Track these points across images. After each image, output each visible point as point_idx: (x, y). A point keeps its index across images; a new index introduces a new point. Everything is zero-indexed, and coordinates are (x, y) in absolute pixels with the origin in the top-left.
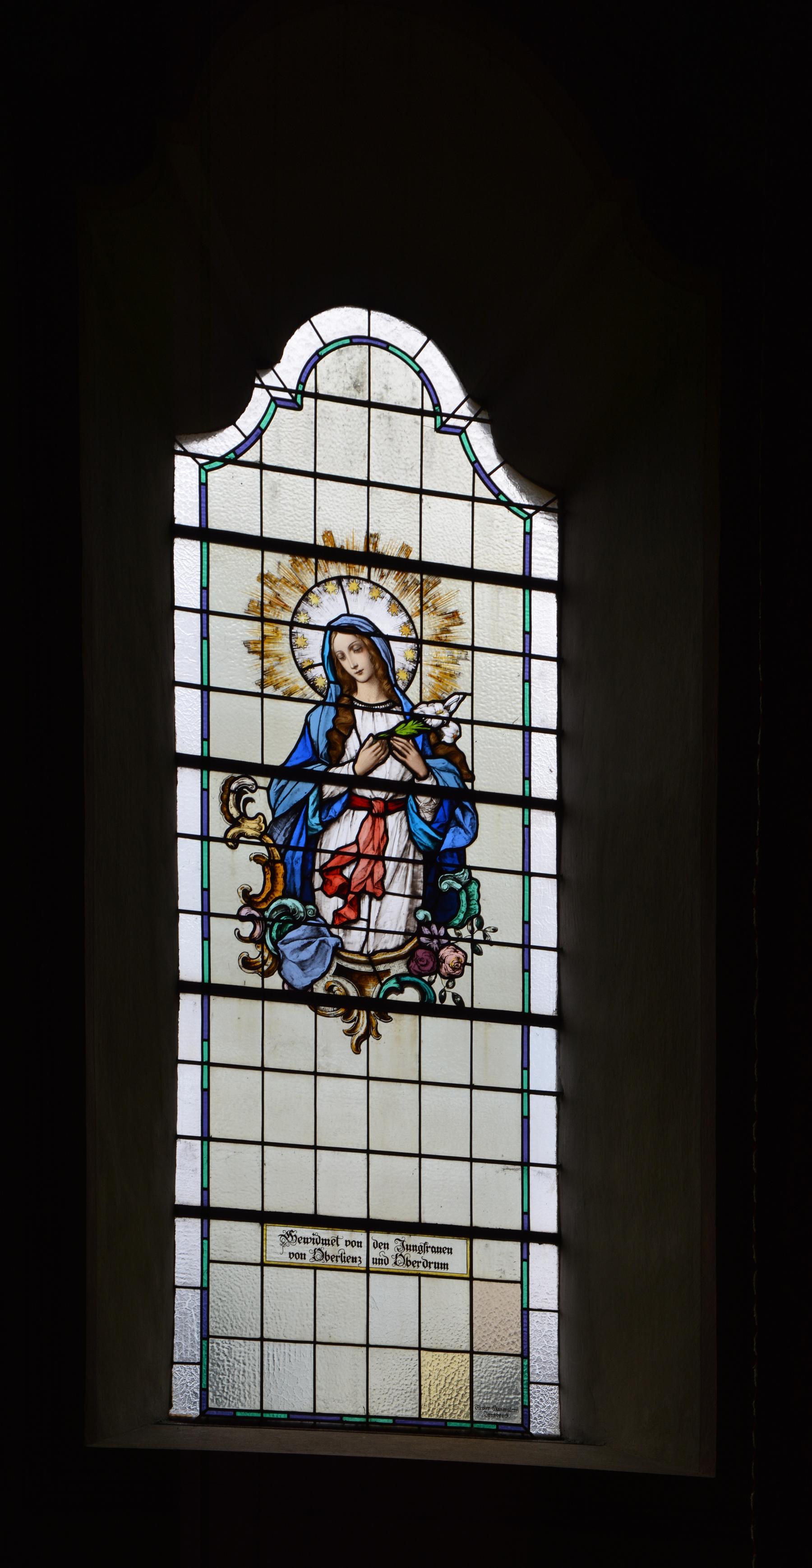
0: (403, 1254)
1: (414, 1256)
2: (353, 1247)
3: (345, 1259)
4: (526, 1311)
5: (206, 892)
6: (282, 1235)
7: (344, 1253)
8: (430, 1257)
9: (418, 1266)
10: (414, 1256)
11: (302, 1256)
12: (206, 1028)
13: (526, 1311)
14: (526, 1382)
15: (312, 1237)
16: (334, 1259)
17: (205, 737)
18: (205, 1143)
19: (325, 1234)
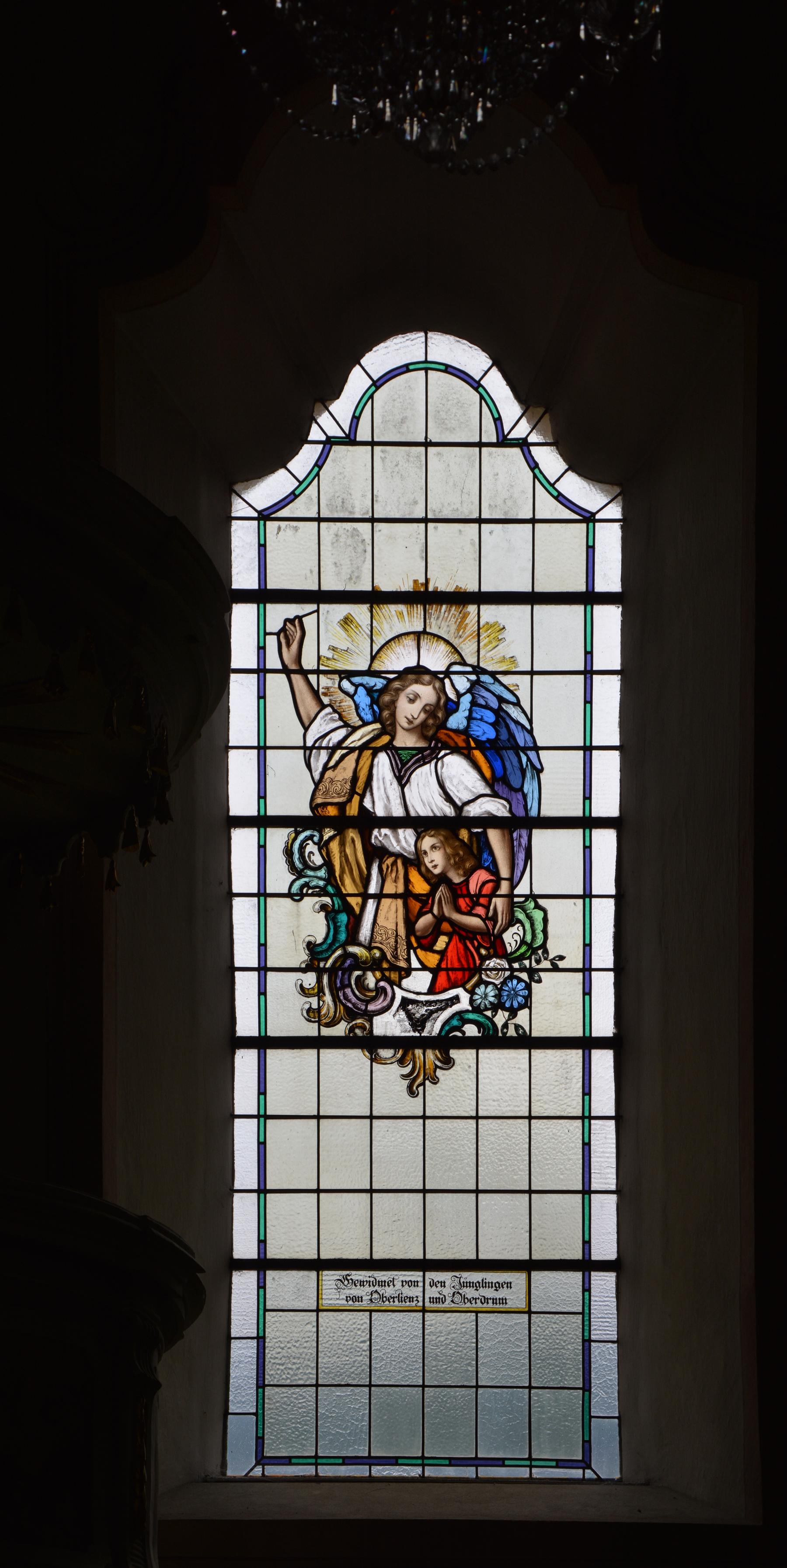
0: (461, 1291)
1: (470, 1293)
2: (410, 1287)
3: (401, 1299)
4: (587, 1342)
5: (262, 947)
6: (339, 1280)
7: (402, 1294)
8: (489, 1293)
9: (476, 1303)
10: (470, 1293)
11: (359, 1299)
12: (262, 1080)
13: (587, 1342)
14: (587, 1417)
15: (368, 1279)
16: (473, 1302)
17: (262, 794)
18: (262, 1196)
19: (382, 1275)
